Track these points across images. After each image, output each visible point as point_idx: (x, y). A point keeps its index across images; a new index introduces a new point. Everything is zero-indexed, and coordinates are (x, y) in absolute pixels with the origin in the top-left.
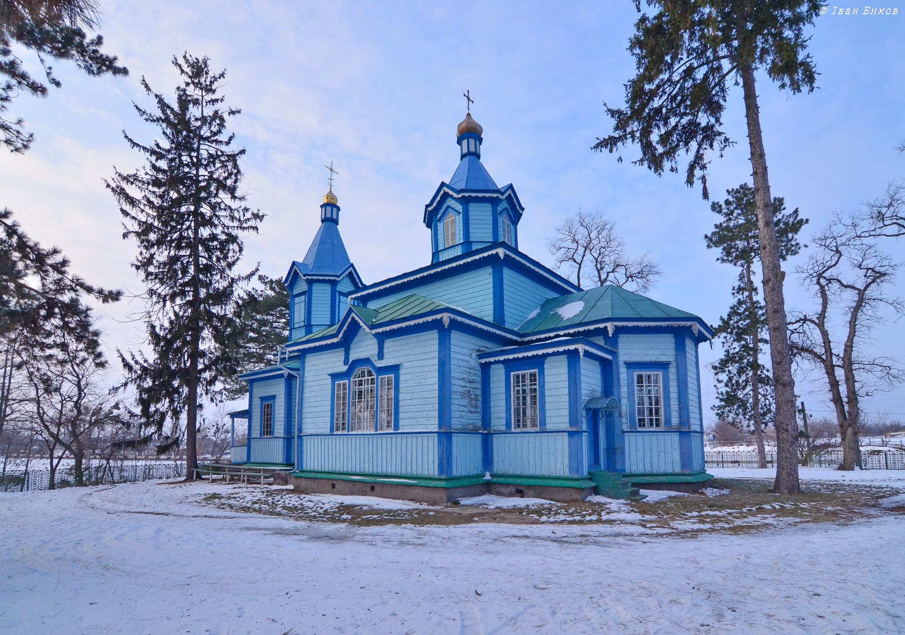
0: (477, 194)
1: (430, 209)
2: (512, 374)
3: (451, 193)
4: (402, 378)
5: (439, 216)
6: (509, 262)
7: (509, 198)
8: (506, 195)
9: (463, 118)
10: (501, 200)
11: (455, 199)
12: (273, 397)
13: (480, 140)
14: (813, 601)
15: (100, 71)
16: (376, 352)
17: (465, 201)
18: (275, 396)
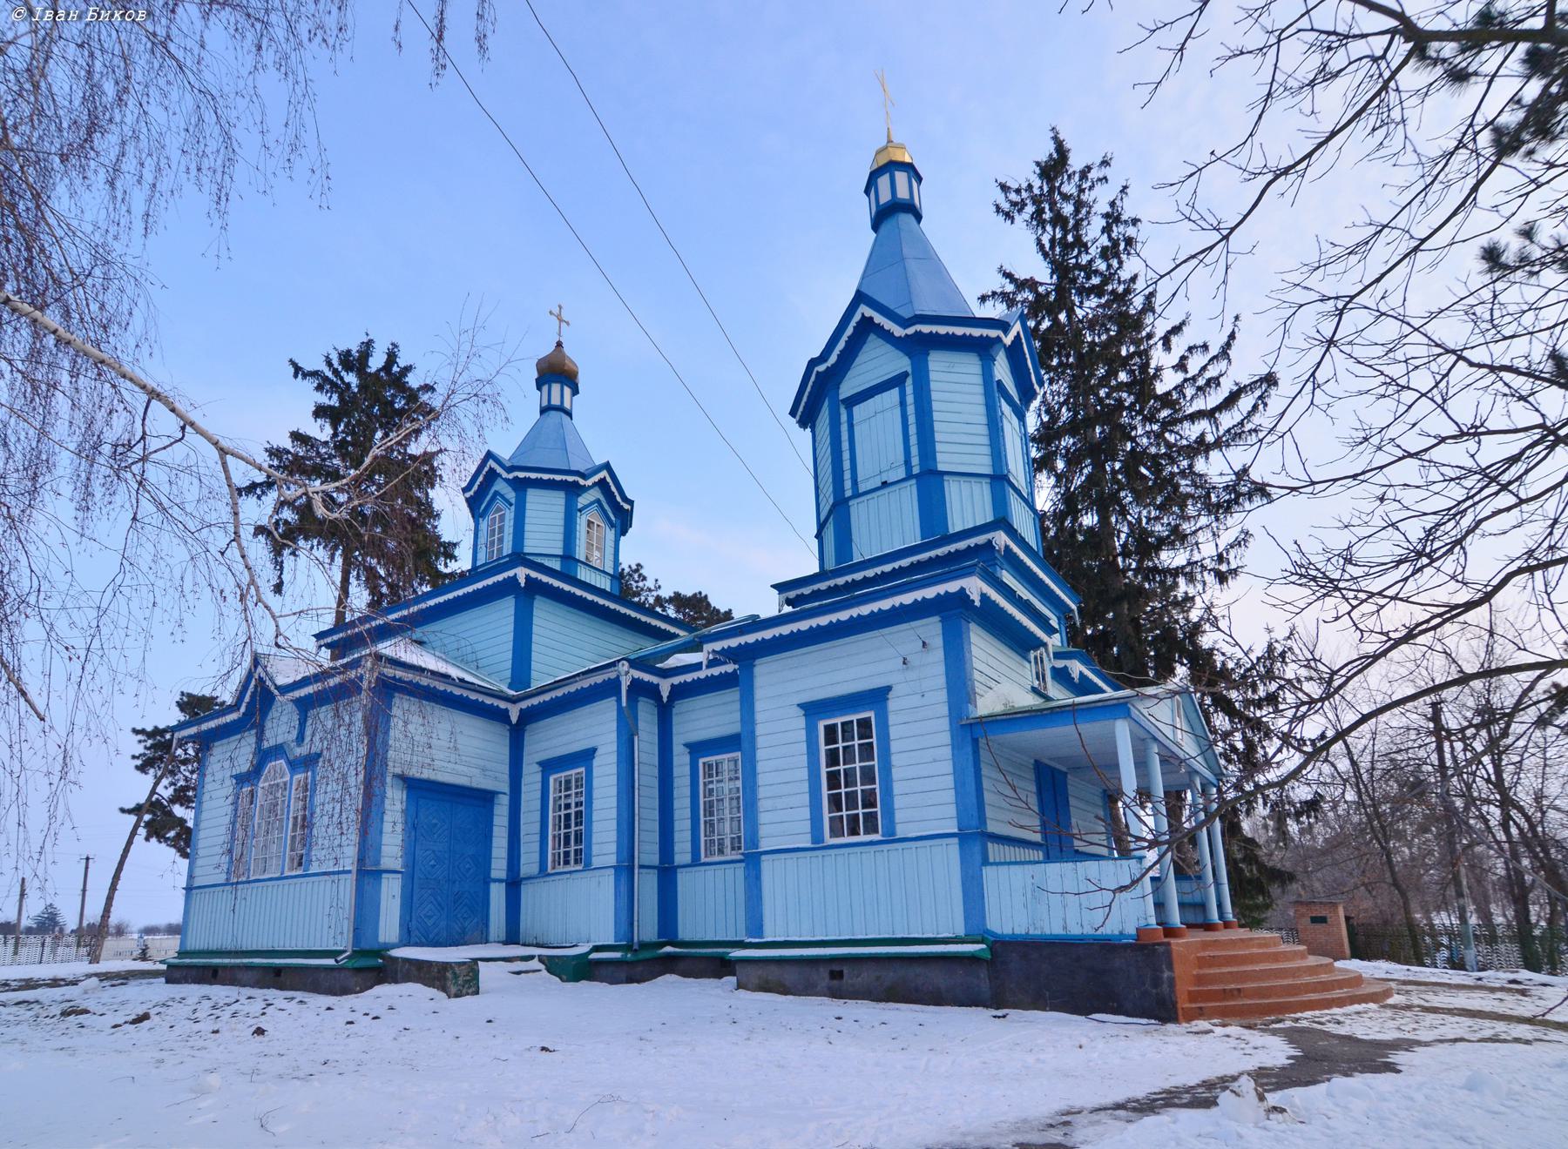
0: (539, 475)
2: (701, 761)
3: (499, 470)
7: (602, 484)
8: (596, 478)
11: (506, 480)
12: (586, 757)
13: (575, 391)
16: (295, 733)
17: (521, 486)
18: (594, 750)
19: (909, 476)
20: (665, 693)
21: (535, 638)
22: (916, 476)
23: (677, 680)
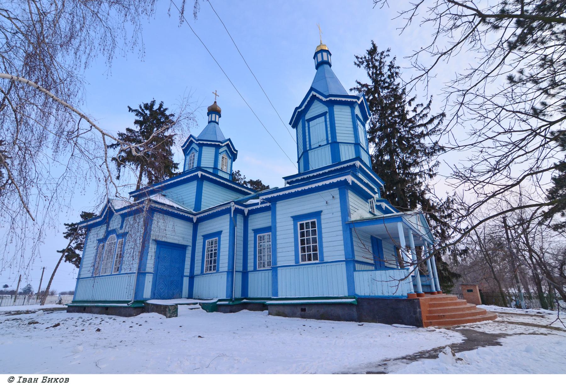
3: (194, 140)
4: (323, 221)
8: (225, 143)
9: (212, 103)
10: (222, 147)
11: (196, 144)
13: (220, 116)
14: (458, 365)
18: (221, 232)
19: (328, 144)
21: (203, 194)
22: (330, 143)
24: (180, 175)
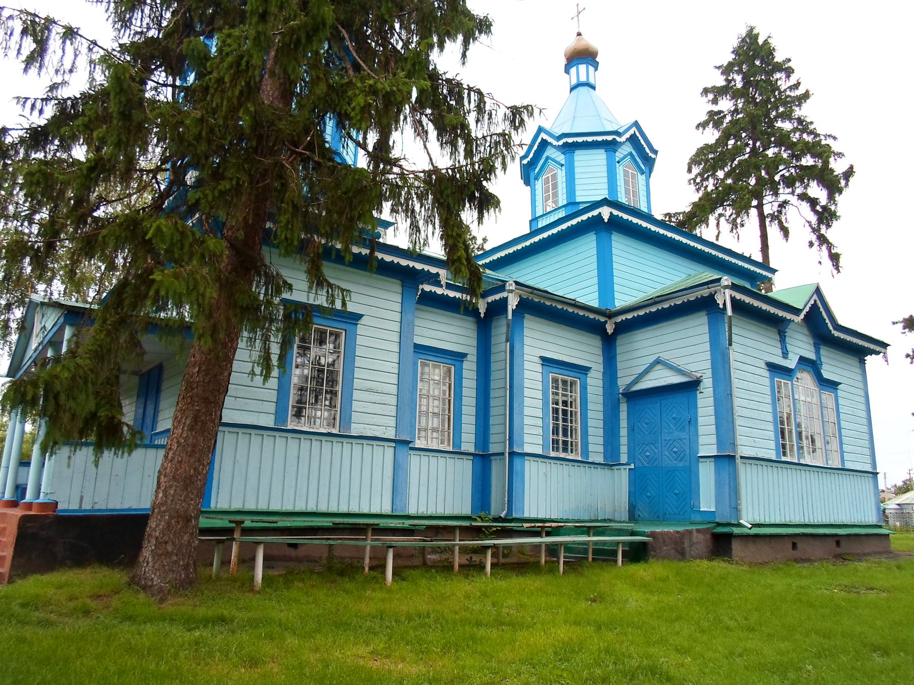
1: (525, 162)
3: (550, 140)
5: (537, 171)
6: (616, 225)
7: (633, 139)
8: (627, 135)
10: (621, 144)
11: (555, 147)
13: (596, 66)
15: (528, 106)
20: (610, 328)
21: (615, 266)
23: (619, 319)
24: (700, 240)
